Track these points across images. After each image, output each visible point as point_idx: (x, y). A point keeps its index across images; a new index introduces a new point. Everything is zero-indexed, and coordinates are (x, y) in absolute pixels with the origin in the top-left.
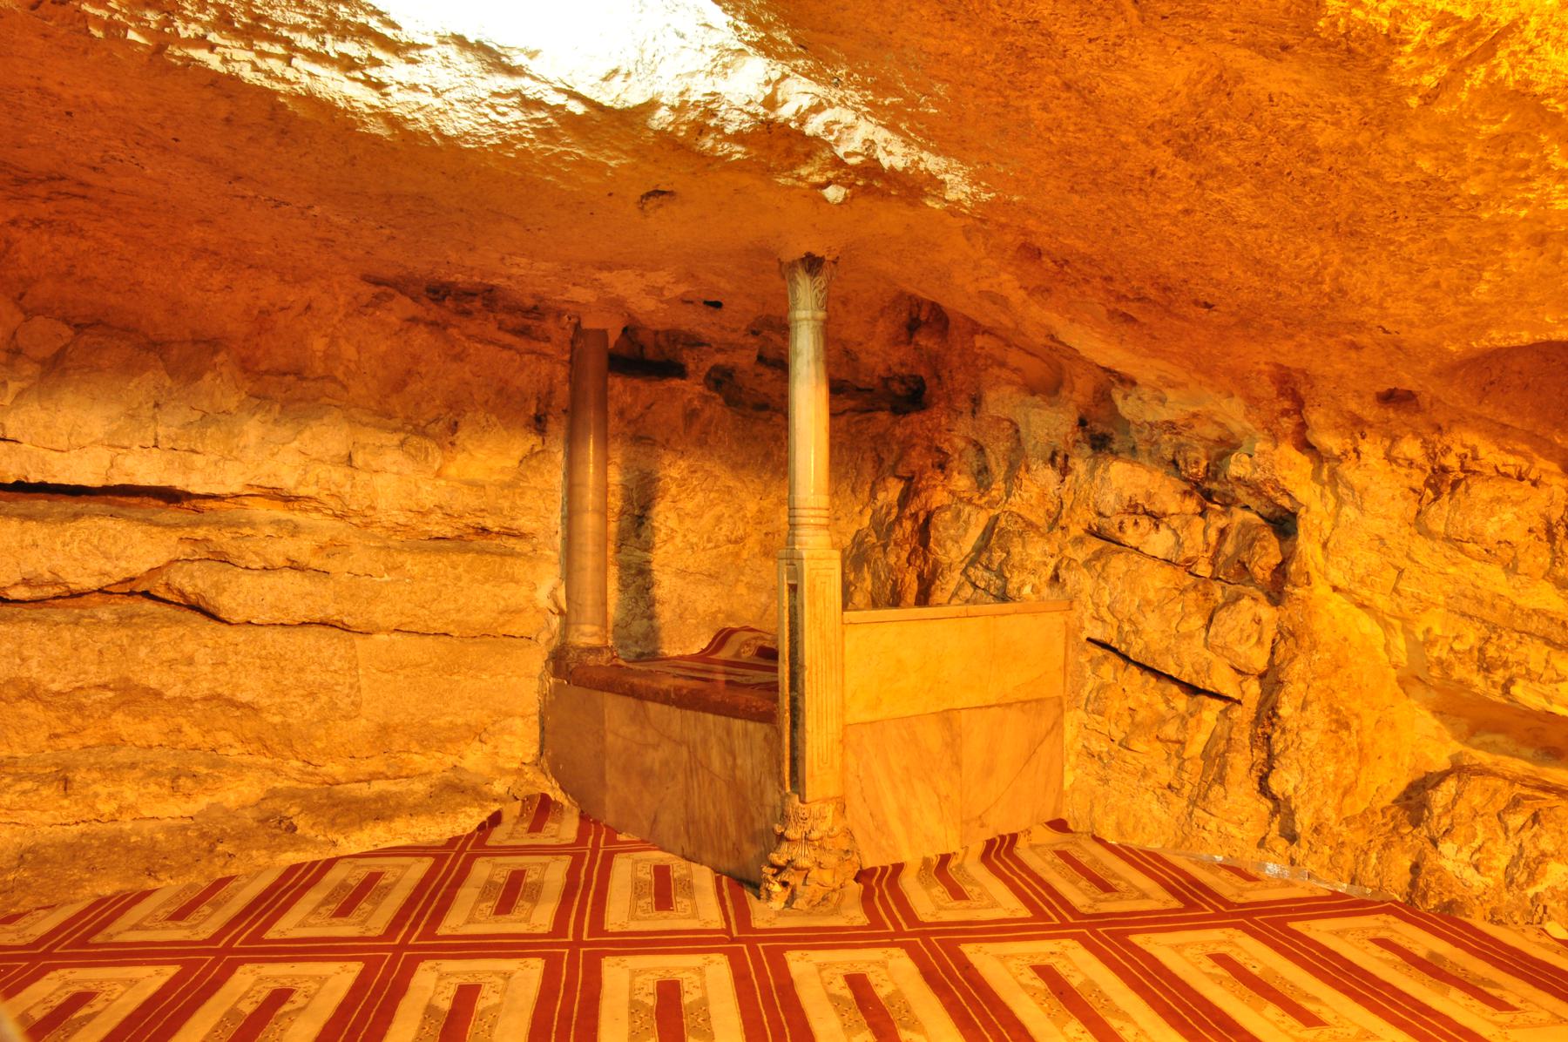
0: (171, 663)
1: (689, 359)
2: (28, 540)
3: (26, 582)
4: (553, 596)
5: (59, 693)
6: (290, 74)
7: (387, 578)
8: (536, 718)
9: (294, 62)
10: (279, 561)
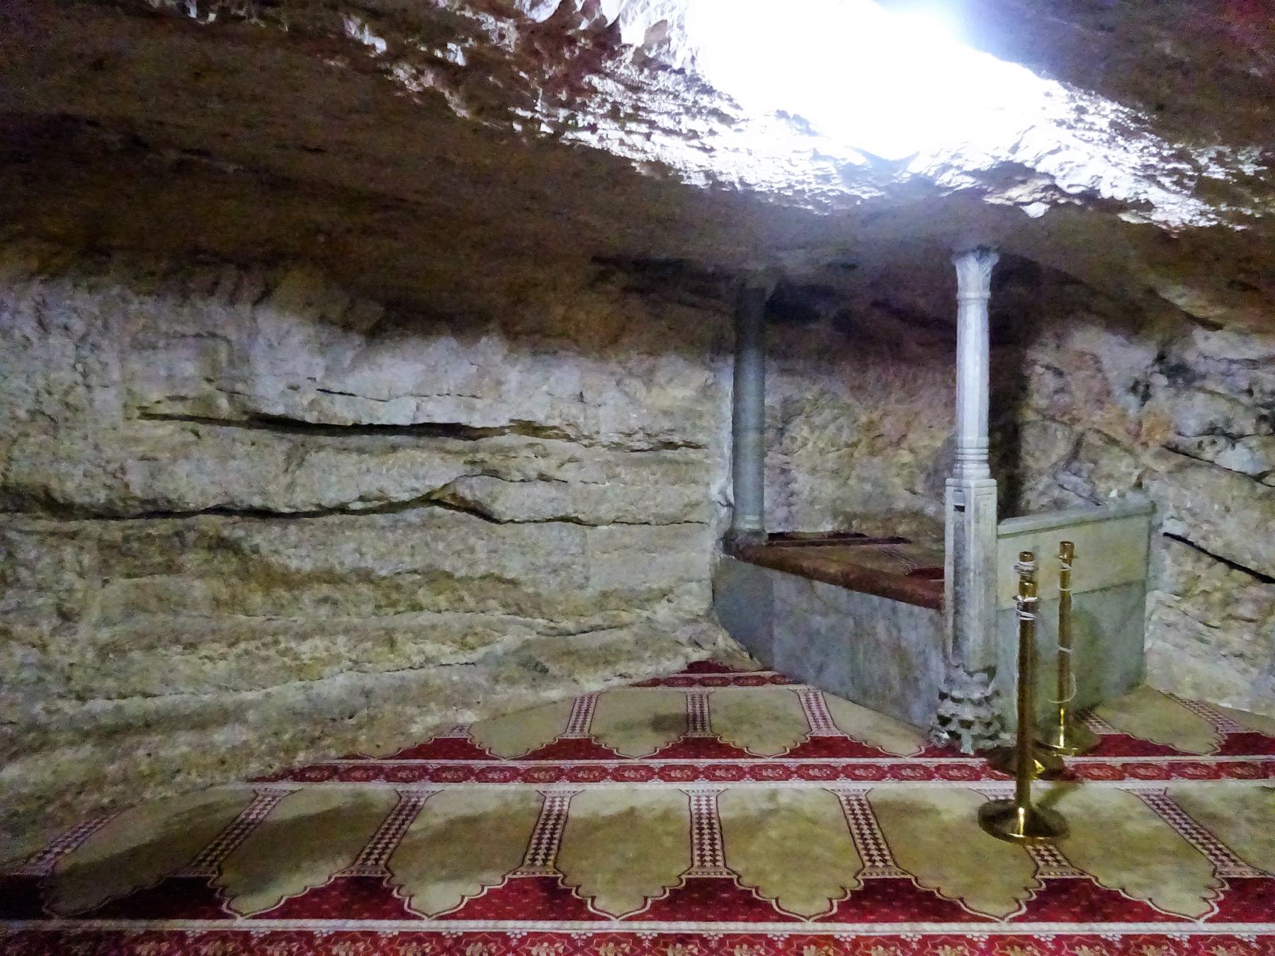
0: (459, 553)
1: (820, 306)
2: (364, 467)
3: (362, 499)
4: (723, 492)
5: (384, 578)
6: (648, 146)
7: (607, 484)
8: (708, 582)
9: (653, 138)
10: (534, 475)
